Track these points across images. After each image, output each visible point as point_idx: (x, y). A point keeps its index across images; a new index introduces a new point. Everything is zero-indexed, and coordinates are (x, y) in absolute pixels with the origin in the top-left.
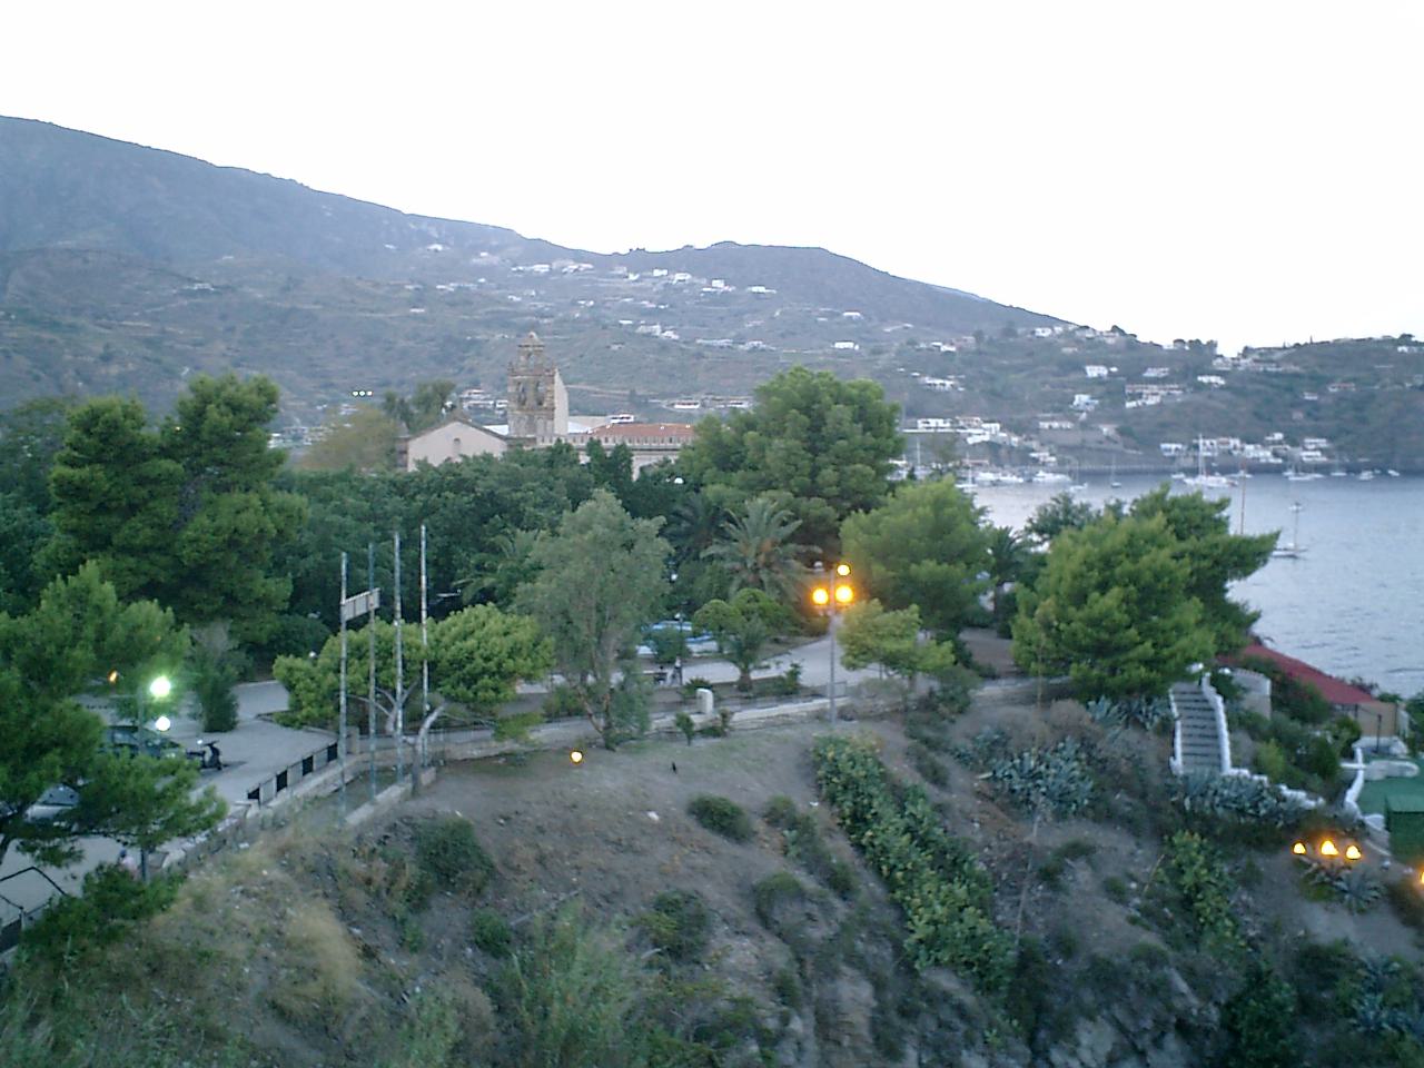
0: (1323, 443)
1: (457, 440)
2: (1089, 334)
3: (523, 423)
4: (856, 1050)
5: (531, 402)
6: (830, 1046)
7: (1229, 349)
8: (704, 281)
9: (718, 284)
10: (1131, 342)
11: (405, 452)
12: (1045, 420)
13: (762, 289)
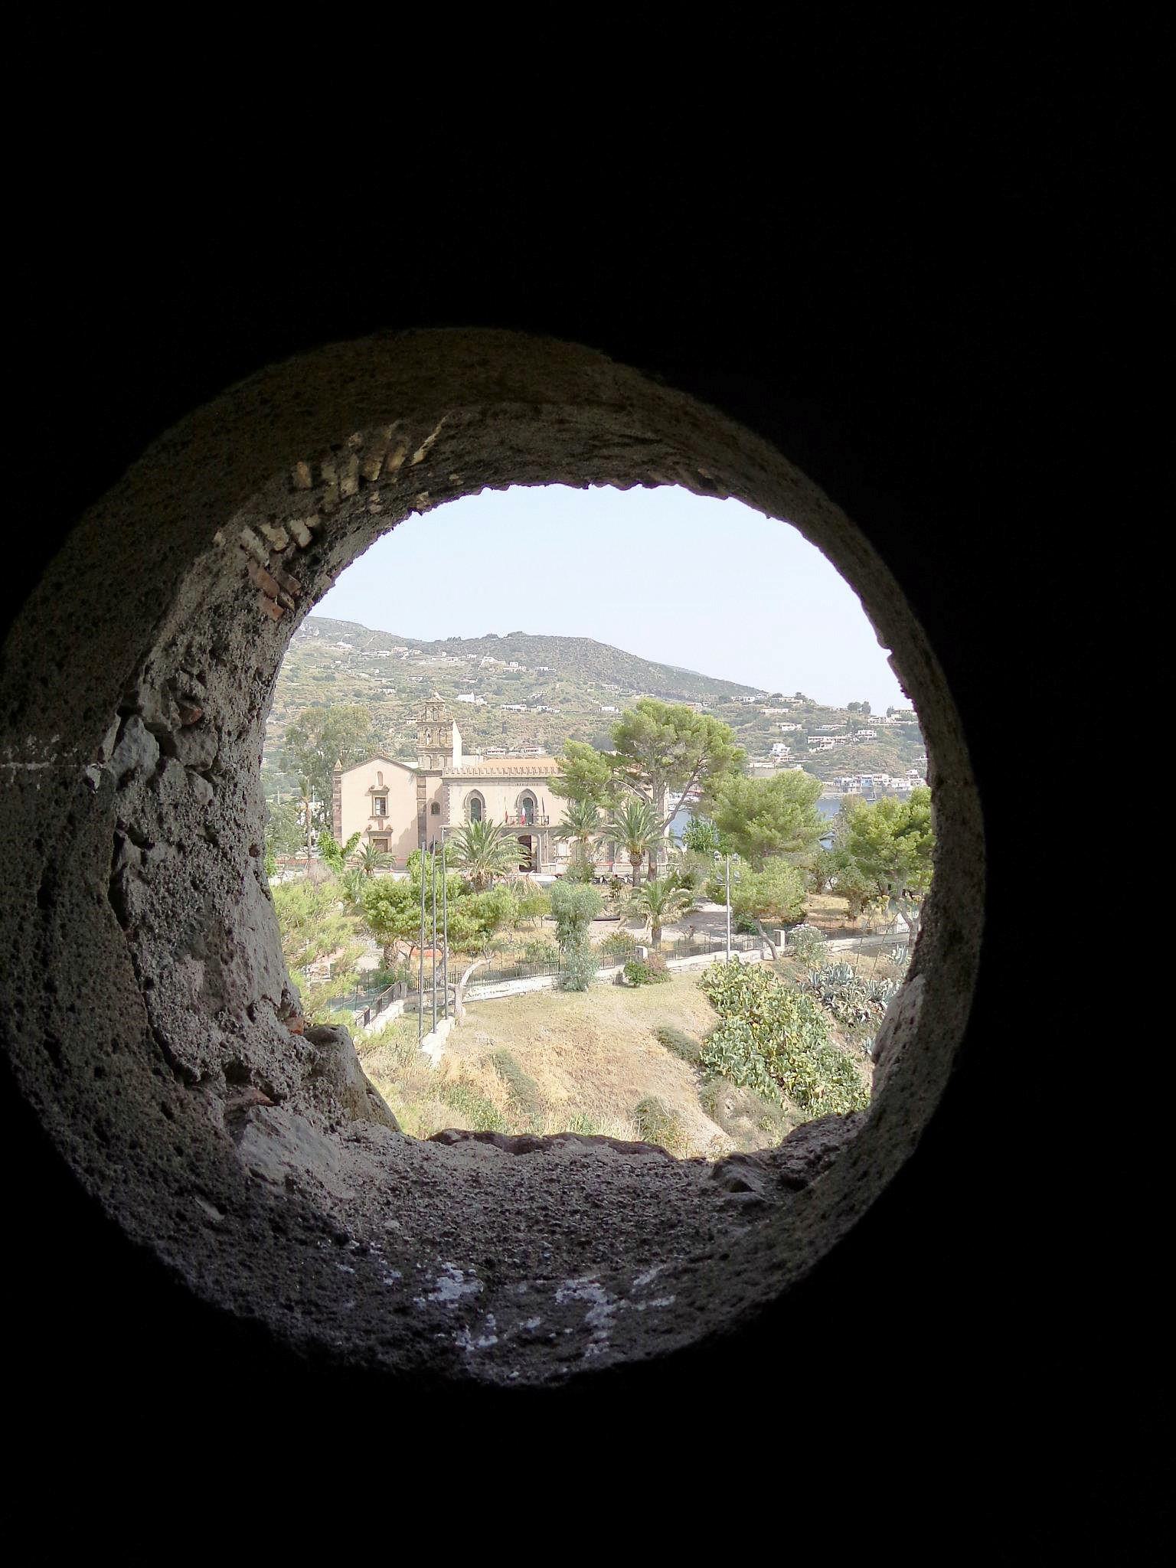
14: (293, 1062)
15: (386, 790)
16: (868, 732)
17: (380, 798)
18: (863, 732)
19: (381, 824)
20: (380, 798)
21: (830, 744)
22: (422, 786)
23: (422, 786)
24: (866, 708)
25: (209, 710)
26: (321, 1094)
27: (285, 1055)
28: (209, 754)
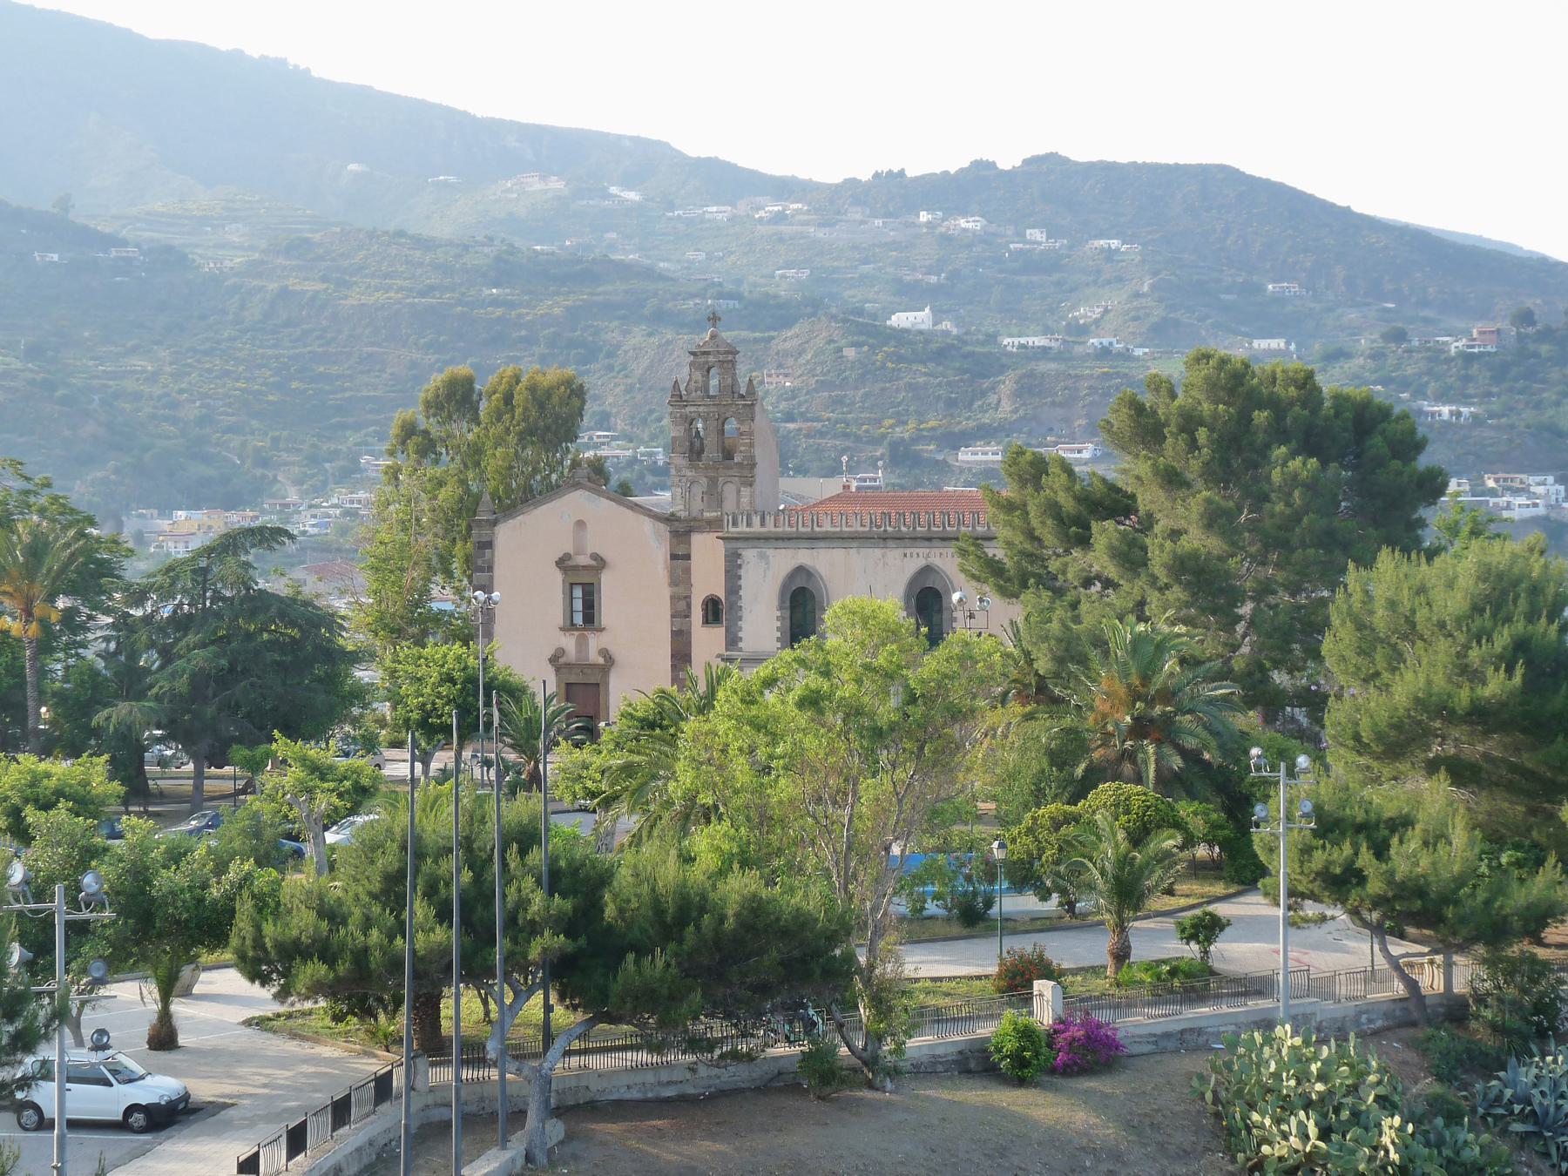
3: (698, 490)
5: (711, 453)
9: (1036, 234)
11: (489, 545)
13: (1114, 243)
15: (600, 563)
19: (582, 644)
22: (680, 557)
23: (680, 557)
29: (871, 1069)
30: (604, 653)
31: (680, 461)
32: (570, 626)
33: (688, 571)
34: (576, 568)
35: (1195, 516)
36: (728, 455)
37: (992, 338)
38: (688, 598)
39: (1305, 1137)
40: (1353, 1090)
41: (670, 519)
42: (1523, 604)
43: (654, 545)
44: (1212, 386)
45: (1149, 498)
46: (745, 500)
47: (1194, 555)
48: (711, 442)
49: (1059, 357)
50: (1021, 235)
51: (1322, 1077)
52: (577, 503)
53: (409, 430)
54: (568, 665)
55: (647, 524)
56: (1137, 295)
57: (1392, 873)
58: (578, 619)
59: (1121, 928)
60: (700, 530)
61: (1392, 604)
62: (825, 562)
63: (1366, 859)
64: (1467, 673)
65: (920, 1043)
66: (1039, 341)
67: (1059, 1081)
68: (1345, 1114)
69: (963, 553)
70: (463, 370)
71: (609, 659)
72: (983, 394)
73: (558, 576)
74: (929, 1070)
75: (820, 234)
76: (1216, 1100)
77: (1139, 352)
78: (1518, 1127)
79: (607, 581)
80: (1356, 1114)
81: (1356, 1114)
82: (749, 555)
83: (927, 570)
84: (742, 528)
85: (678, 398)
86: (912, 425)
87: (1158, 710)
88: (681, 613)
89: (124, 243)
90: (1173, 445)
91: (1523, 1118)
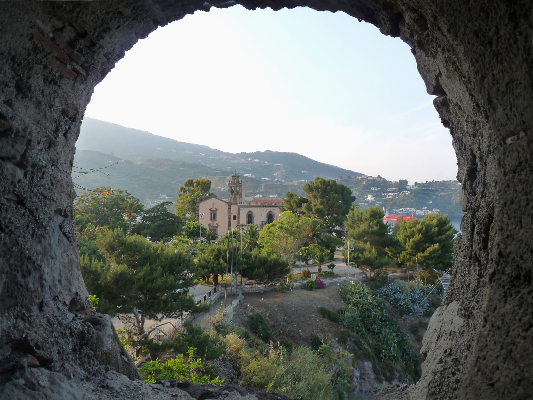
0: (438, 210)
1: (213, 203)
2: (371, 178)
3: (233, 198)
4: (369, 381)
5: (235, 192)
6: (362, 380)
7: (411, 183)
8: (263, 162)
9: (267, 162)
10: (384, 181)
11: (199, 206)
12: (360, 202)
13: (279, 164)
14: (67, 338)
15: (216, 210)
16: (407, 191)
17: (214, 214)
18: (405, 191)
19: (213, 223)
20: (214, 214)
21: (390, 195)
22: (230, 209)
23: (230, 209)
24: (406, 182)
25: (16, 124)
26: (84, 356)
27: (62, 333)
28: (18, 151)
29: (289, 288)
30: (217, 224)
31: (230, 194)
32: (211, 220)
33: (231, 211)
34: (213, 210)
35: (319, 202)
36: (238, 193)
37: (260, 178)
38: (231, 215)
39: (357, 298)
40: (363, 291)
41: (228, 203)
42: (378, 216)
43: (225, 207)
44: (321, 183)
45: (312, 200)
46: (240, 200)
47: (319, 209)
48: (235, 191)
49: (271, 181)
50: (264, 163)
51: (358, 289)
52: (212, 200)
53: (182, 188)
54: (211, 226)
55: (224, 203)
56: (282, 172)
57: (364, 257)
58: (213, 219)
59: (320, 266)
60: (233, 205)
61: (358, 216)
62: (254, 210)
63: (360, 255)
64: (370, 226)
65: (296, 284)
66: (268, 179)
67: (317, 290)
68: (362, 295)
69: (280, 208)
70: (191, 179)
71: (218, 225)
72: (259, 187)
73: (210, 212)
74: (297, 288)
75: (233, 161)
76: (341, 293)
77: (283, 181)
78: (384, 297)
79: (217, 212)
80: (364, 295)
81: (364, 295)
82: (242, 209)
83: (270, 211)
84: (241, 204)
85: (230, 184)
86: (248, 191)
87: (317, 233)
88: (229, 218)
89: (121, 160)
90: (315, 192)
91: (385, 295)
